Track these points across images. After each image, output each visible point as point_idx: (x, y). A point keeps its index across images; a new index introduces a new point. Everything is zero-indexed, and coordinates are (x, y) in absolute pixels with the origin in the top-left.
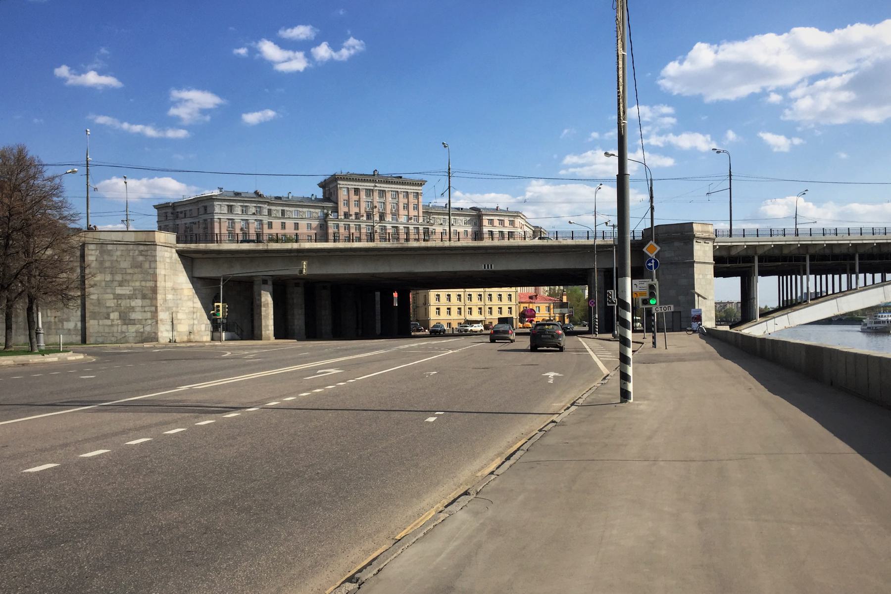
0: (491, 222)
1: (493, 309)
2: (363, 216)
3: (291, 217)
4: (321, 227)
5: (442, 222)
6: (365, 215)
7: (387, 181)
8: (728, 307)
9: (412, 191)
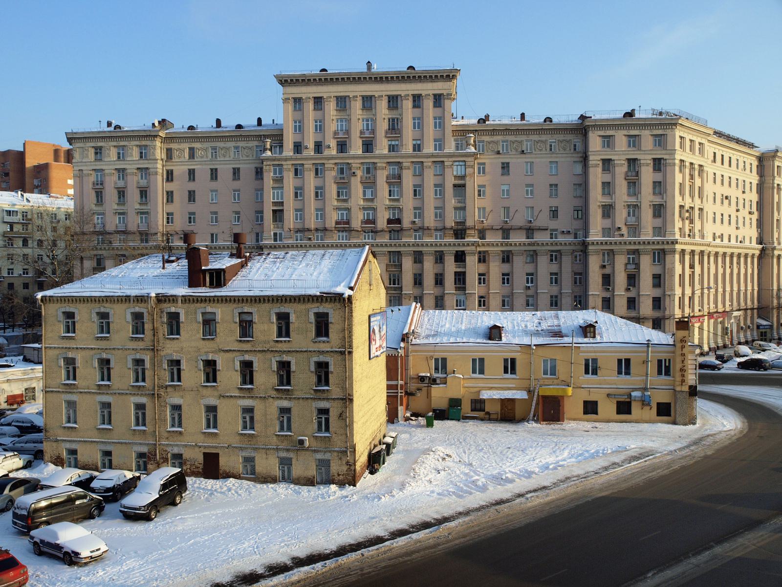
0: (608, 141)
6: (333, 144)
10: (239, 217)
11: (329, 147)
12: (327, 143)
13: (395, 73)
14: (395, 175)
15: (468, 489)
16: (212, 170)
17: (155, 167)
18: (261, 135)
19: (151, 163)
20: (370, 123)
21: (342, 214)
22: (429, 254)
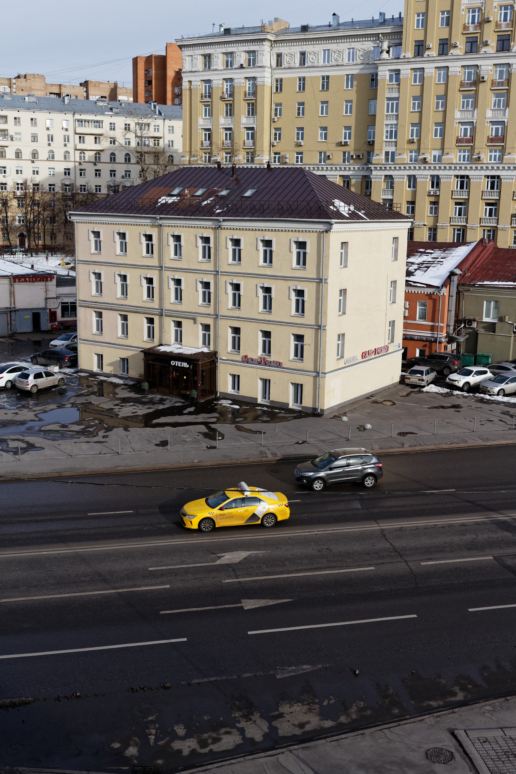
2: (486, 44)
10: (326, 134)
11: (486, 44)
12: (453, 42)
15: (248, 553)
17: (263, 76)
18: (379, 34)
20: (477, 14)
21: (497, 129)
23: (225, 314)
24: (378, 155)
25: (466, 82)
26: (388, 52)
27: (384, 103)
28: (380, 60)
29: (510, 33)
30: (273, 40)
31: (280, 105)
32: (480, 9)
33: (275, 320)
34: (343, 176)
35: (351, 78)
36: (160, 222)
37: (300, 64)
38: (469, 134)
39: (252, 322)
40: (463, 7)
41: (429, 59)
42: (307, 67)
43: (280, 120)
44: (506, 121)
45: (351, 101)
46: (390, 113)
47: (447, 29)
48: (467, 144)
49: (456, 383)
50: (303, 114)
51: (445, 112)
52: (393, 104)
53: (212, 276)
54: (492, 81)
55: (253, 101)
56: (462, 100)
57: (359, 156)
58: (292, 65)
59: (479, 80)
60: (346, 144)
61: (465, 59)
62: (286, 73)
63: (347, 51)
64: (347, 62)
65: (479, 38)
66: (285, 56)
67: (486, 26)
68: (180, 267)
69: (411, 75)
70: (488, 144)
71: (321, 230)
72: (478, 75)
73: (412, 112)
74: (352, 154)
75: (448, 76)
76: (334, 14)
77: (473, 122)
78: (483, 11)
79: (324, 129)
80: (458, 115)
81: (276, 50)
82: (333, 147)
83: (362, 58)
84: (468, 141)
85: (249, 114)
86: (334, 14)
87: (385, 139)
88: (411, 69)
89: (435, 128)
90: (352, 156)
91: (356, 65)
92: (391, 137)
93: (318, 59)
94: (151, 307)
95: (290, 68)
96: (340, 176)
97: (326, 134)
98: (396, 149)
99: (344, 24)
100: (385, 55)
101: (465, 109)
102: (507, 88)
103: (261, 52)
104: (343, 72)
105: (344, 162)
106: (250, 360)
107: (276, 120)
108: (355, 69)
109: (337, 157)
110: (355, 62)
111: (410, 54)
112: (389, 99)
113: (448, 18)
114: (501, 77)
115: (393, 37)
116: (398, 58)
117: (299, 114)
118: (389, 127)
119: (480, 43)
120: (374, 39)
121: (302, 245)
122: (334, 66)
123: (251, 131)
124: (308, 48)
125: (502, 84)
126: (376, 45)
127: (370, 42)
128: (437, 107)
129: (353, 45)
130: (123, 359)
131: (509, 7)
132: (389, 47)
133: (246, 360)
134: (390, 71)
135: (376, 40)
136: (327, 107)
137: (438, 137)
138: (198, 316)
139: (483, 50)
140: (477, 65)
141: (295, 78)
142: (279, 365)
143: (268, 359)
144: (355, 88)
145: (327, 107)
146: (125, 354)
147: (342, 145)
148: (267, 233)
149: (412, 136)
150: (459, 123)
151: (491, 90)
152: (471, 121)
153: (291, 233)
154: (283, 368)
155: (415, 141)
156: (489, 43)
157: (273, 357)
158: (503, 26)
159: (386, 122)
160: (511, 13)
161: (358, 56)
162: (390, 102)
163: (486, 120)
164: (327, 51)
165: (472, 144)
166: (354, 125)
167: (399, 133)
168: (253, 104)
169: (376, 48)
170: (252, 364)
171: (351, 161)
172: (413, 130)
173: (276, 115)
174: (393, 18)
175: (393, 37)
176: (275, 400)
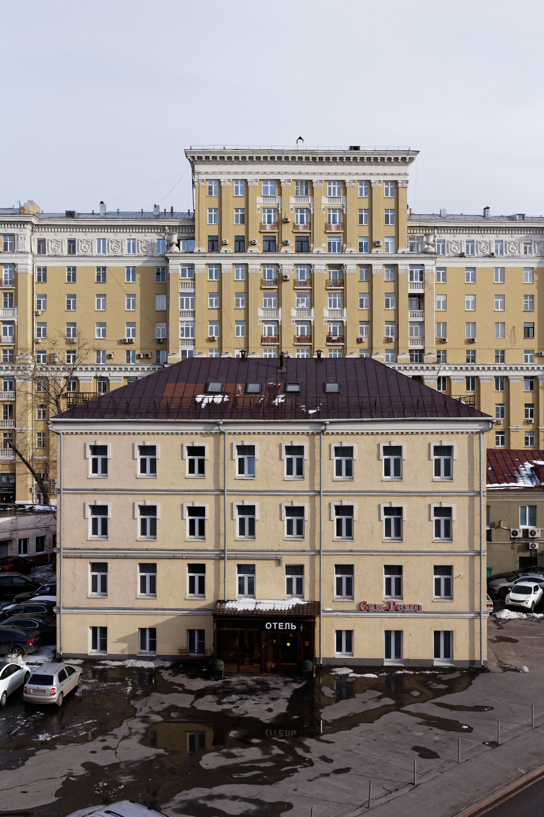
1: (357, 572)
2: (286, 244)
3: (89, 253)
4: (158, 274)
5: (464, 250)
6: (259, 240)
7: (314, 159)
8: (274, 664)
9: (382, 178)
10: (104, 331)
13: (325, 152)
14: (336, 280)
16: (98, 269)
18: (165, 226)
19: (20, 258)
21: (303, 329)
22: (517, 377)
23: (329, 549)
24: (174, 354)
25: (267, 280)
26: (178, 245)
27: (178, 299)
28: (171, 253)
29: (308, 235)
30: (36, 224)
31: (45, 296)
32: (276, 210)
33: (409, 549)
34: (127, 377)
35: (132, 271)
36: (223, 428)
37: (69, 252)
38: (273, 334)
39: (373, 555)
40: (258, 206)
41: (227, 255)
42: (78, 256)
43: (45, 313)
44: (312, 320)
45: (134, 296)
46: (185, 309)
47: (243, 227)
48: (273, 344)
49: (524, 604)
50: (74, 307)
51: (247, 310)
52: (187, 300)
53: (307, 498)
54: (294, 280)
55: (12, 291)
56: (296, 298)
57: (147, 355)
58: (59, 252)
59: (281, 279)
60: (131, 342)
61: (265, 257)
62: (52, 261)
63: (127, 241)
64: (127, 253)
65: (277, 237)
66: (50, 242)
67: (284, 226)
68: (252, 489)
69: (207, 271)
70: (295, 344)
71: (475, 431)
72: (278, 273)
73: (209, 309)
74: (138, 352)
75: (247, 274)
76: (102, 203)
77: (278, 321)
78: (280, 212)
79: (103, 324)
80: (261, 313)
81: (38, 235)
82: (115, 345)
83: (145, 250)
84: (274, 340)
85: (5, 306)
86: (102, 203)
87: (180, 338)
88: (206, 264)
89: (126, 328)
90: (139, 355)
91: (138, 256)
92: (187, 335)
93: (92, 248)
94: (201, 548)
95: (55, 256)
96: (125, 377)
97: (104, 331)
98: (195, 348)
99: (110, 213)
100: (175, 248)
101: (267, 308)
102: (311, 288)
103: (22, 236)
104: (123, 264)
105: (128, 361)
106: (372, 608)
107: (40, 313)
108: (137, 261)
109: (120, 356)
110: (137, 254)
111: (204, 249)
112: (182, 294)
113: (242, 216)
114: (302, 276)
115: (184, 231)
116: (192, 252)
117: (69, 307)
118: (185, 323)
119: (279, 243)
120: (159, 231)
121: (446, 451)
122: (81, 256)
123: (10, 326)
124: (78, 236)
125: (305, 284)
126: (161, 238)
127: (154, 234)
128: (237, 304)
129: (134, 236)
130: (143, 631)
131: (305, 210)
132: (179, 241)
133: (364, 608)
134: (182, 265)
135: (160, 232)
136: (104, 301)
137: (240, 336)
138: (283, 555)
139: (283, 249)
140: (310, 265)
141: (64, 267)
142: (417, 609)
143: (398, 602)
144: (138, 281)
145: (104, 301)
146: (148, 622)
147: (125, 343)
148: (444, 437)
149: (211, 333)
150: (263, 321)
151: (294, 289)
152: (276, 319)
153: (429, 436)
154: (425, 612)
155: (216, 339)
156: (289, 243)
157: (408, 599)
158: (301, 228)
159: (181, 319)
160: (307, 216)
161: (140, 248)
162: (185, 298)
163: (292, 319)
164: (101, 240)
165: (278, 344)
166: (139, 321)
167: (196, 330)
168: (11, 294)
169: (161, 241)
170: (375, 612)
171: (138, 361)
172: (211, 328)
173: (39, 307)
174: (142, 212)
175: (187, 231)
176: (411, 658)
